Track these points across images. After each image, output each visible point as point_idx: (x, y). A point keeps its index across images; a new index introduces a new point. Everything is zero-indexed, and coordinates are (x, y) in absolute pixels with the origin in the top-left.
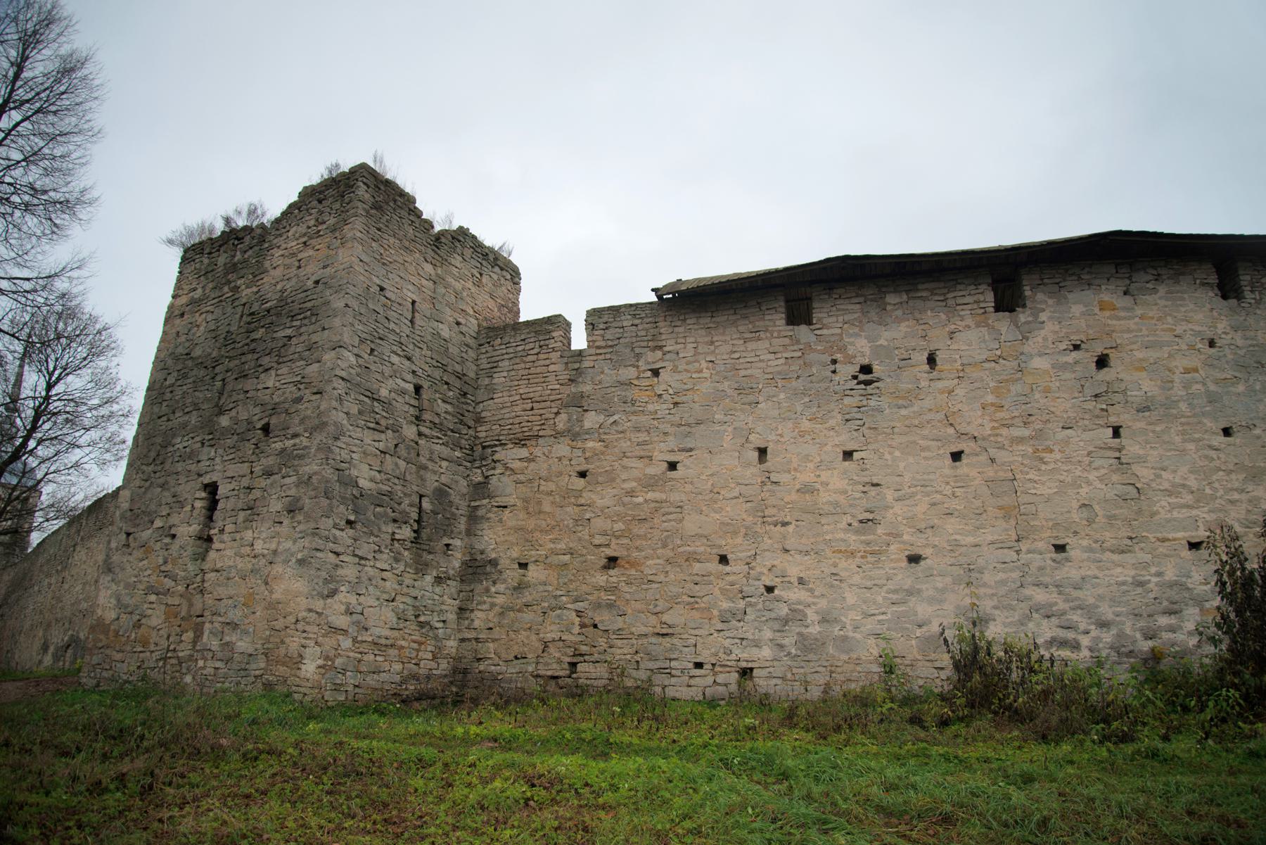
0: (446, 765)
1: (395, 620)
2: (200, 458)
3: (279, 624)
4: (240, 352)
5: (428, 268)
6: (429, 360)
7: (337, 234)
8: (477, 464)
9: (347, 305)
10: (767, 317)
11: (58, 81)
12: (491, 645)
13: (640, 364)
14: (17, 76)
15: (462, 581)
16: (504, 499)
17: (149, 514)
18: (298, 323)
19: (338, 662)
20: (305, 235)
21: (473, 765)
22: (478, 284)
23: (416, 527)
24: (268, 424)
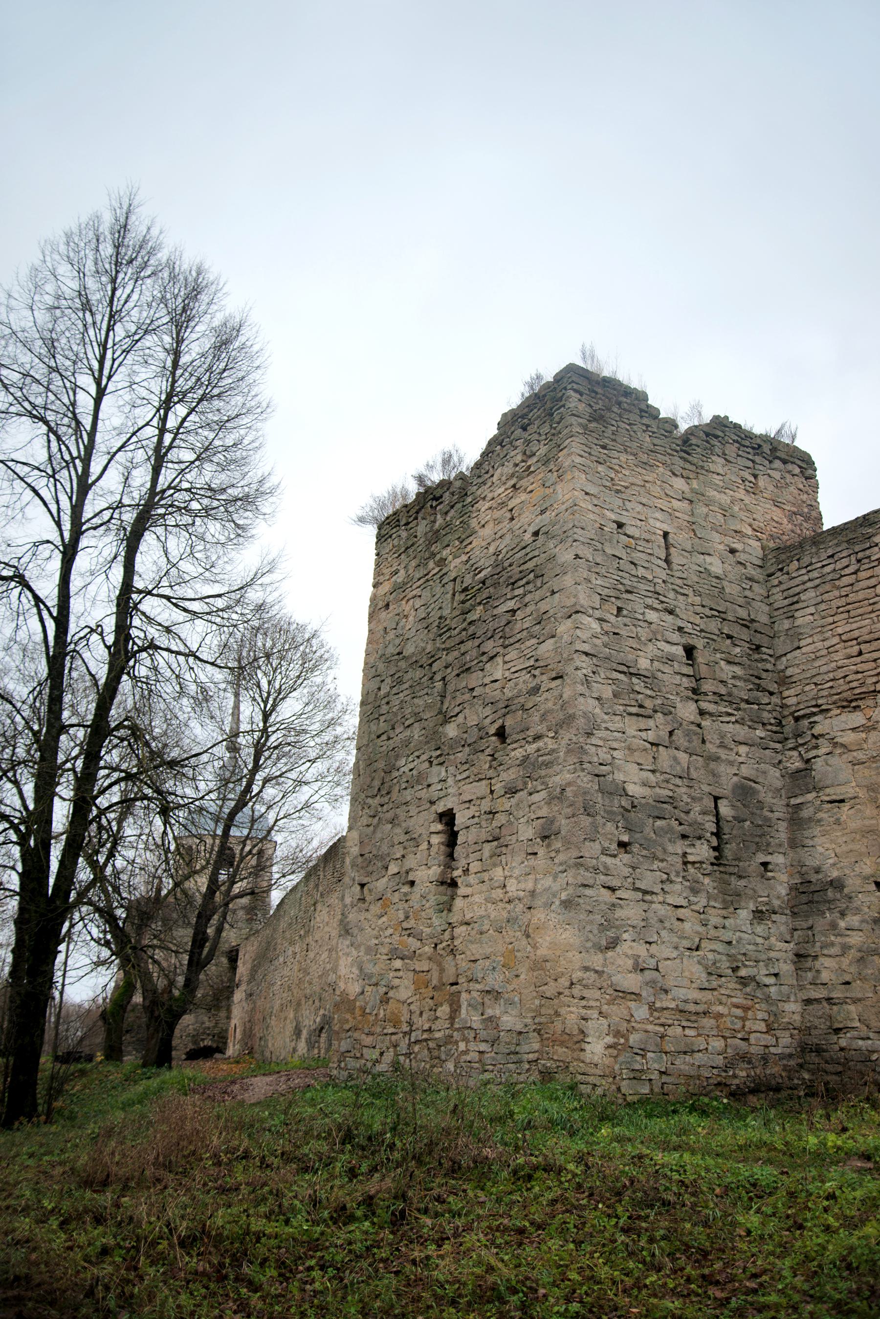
0: (792, 1195)
1: (704, 975)
2: (430, 781)
3: (550, 990)
4: (457, 640)
5: (679, 484)
6: (699, 609)
7: (552, 466)
8: (791, 744)
9: (577, 556)
11: (217, 358)
12: (852, 1008)
14: (175, 364)
15: (794, 914)
16: (839, 790)
17: (382, 858)
18: (520, 591)
19: (634, 1039)
20: (512, 475)
21: (831, 1197)
22: (754, 490)
23: (715, 843)
24: (503, 727)
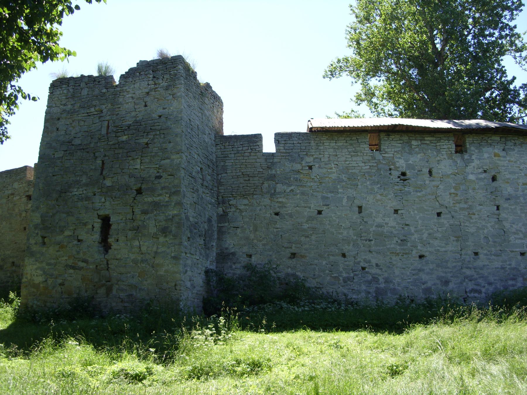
8: (221, 205)
10: (361, 146)
13: (303, 162)
15: (217, 262)
24: (141, 188)
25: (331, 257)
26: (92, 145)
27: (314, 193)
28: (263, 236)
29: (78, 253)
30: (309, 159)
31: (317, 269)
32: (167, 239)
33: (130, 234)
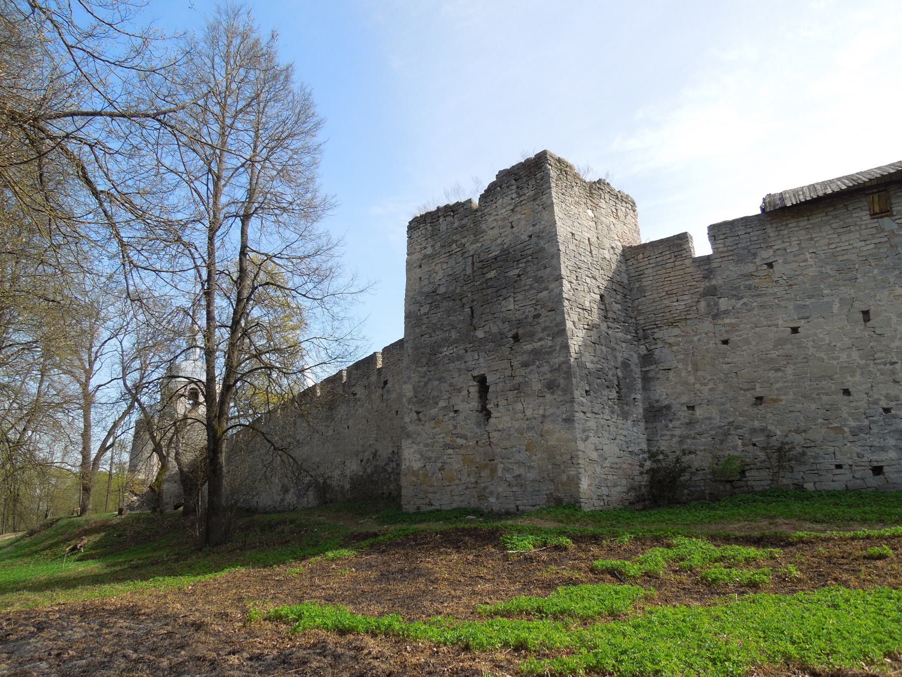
2: (466, 359)
8: (642, 342)
10: (855, 215)
13: (757, 260)
15: (646, 422)
24: (517, 334)
25: (824, 398)
26: (458, 291)
27: (782, 303)
28: (709, 378)
29: (455, 427)
30: (767, 254)
31: (802, 418)
32: (556, 397)
33: (511, 395)
